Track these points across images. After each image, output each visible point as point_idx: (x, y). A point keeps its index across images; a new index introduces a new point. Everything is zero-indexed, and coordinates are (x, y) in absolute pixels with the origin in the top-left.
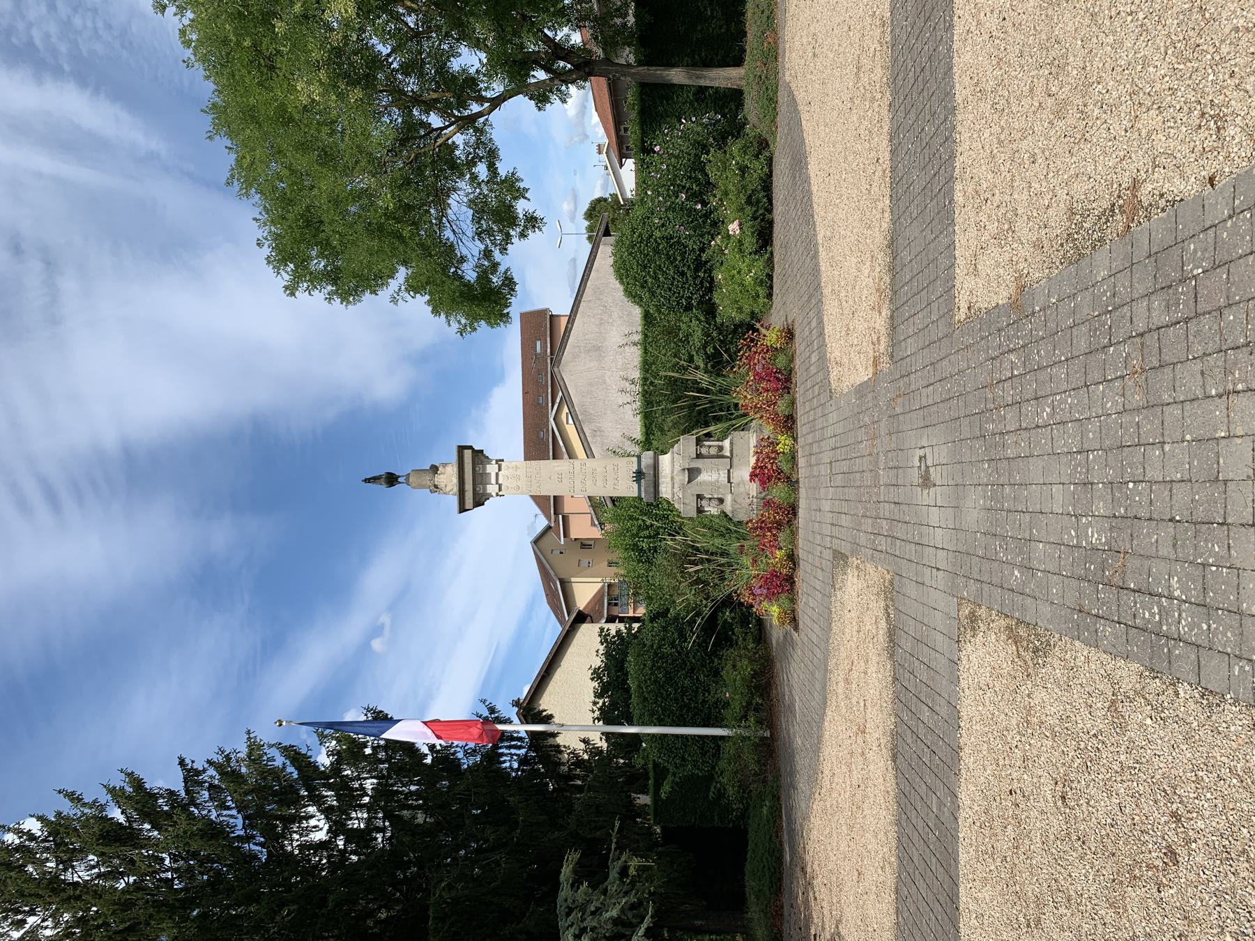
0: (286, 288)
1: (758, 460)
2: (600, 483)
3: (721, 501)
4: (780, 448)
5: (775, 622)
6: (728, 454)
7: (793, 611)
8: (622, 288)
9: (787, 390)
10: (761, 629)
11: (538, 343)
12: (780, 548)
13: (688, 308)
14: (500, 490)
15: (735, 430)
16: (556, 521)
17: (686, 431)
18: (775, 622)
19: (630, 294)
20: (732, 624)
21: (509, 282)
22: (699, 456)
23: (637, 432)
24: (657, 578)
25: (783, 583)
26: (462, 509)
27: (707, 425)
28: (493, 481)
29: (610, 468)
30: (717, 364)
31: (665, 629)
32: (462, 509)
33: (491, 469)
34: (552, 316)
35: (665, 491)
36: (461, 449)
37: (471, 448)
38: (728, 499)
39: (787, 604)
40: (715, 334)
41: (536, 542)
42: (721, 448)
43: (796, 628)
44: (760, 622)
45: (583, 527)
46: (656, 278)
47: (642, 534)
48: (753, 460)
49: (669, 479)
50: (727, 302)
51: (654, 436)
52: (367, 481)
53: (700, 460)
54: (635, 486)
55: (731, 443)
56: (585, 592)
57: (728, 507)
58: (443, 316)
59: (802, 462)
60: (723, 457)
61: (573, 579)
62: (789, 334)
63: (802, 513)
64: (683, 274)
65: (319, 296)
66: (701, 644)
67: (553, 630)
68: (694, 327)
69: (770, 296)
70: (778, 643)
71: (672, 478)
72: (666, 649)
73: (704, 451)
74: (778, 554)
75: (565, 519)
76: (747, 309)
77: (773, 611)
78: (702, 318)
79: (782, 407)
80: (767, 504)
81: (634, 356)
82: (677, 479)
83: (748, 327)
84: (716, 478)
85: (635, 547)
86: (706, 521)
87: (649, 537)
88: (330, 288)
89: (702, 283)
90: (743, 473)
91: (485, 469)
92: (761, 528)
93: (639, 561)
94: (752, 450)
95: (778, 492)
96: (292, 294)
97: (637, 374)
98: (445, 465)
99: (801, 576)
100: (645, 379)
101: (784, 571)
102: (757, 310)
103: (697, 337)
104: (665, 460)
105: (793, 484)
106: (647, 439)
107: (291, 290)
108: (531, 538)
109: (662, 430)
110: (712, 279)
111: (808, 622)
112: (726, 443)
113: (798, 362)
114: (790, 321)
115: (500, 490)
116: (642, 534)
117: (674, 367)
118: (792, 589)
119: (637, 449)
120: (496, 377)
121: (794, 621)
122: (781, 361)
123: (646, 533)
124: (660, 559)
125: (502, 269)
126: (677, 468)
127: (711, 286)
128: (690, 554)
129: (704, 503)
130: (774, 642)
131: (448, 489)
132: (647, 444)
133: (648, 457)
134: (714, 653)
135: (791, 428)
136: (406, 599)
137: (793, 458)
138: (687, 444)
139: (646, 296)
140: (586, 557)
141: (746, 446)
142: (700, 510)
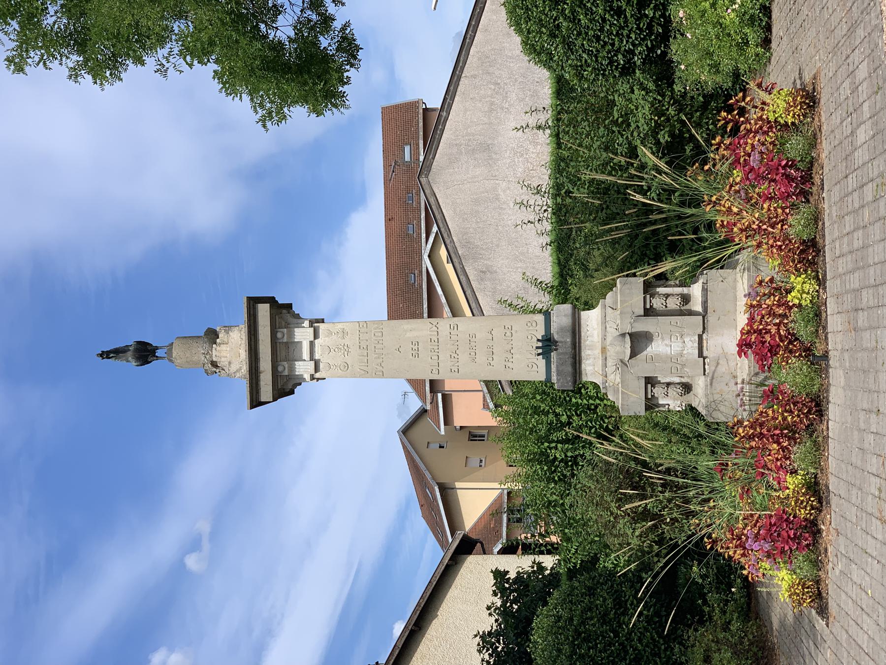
0: (10, 60)
1: (751, 319)
2: (481, 358)
3: (687, 388)
4: (793, 298)
5: (783, 595)
6: (698, 308)
7: (818, 582)
8: (518, 39)
9: (805, 195)
10: (751, 602)
11: (407, 149)
12: (794, 472)
13: (627, 70)
14: (317, 369)
15: (711, 267)
16: (434, 401)
17: (627, 267)
18: (783, 595)
19: (533, 49)
20: (702, 586)
21: (349, 47)
22: (649, 312)
23: (547, 272)
24: (581, 508)
25: (800, 534)
26: (256, 402)
27: (658, 259)
28: (306, 355)
29: (498, 333)
30: (680, 151)
31: (591, 591)
32: (256, 402)
33: (303, 335)
34: (426, 110)
35: (591, 371)
36: (253, 302)
37: (271, 301)
38: (700, 385)
39: (806, 570)
40: (672, 111)
41: (405, 431)
42: (686, 299)
43: (823, 611)
44: (749, 586)
45: (471, 411)
46: (574, 20)
47: (554, 437)
48: (742, 320)
49: (598, 351)
50: (693, 57)
51: (573, 280)
52: (105, 355)
53: (651, 320)
54: (541, 362)
55: (705, 291)
56: (476, 501)
57: (699, 398)
58: (246, 98)
59: (834, 322)
60: (691, 313)
61: (458, 485)
62: (808, 99)
63: (834, 412)
64: (619, 12)
65: (60, 69)
66: (654, 620)
67: (431, 555)
68: (638, 102)
69: (766, 42)
70: (782, 623)
71: (604, 350)
72: (593, 626)
73: (657, 303)
74: (792, 482)
75: (446, 399)
76: (727, 65)
77: (780, 582)
78: (651, 86)
79: (797, 225)
80: (771, 395)
81: (539, 151)
82: (612, 352)
83: (723, 103)
84: (686, 349)
85: (542, 458)
86: (658, 418)
87: (566, 441)
88: (75, 57)
89: (650, 27)
90: (725, 340)
91: (291, 335)
92: (761, 436)
93: (550, 480)
94: (742, 302)
95: (791, 374)
96: (20, 69)
97: (543, 177)
98: (228, 328)
99: (832, 525)
100: (558, 188)
101: (802, 514)
102: (742, 67)
103: (643, 115)
104: (591, 319)
105: (818, 362)
106: (561, 284)
107: (17, 64)
108: (400, 424)
109: (585, 269)
110: (668, 21)
111: (850, 607)
112: (696, 290)
113: (825, 148)
114: (807, 78)
115: (317, 369)
116: (554, 437)
117: (603, 167)
118: (815, 543)
119: (543, 300)
120: (358, 200)
121: (819, 600)
122: (795, 146)
123: (561, 435)
124: (584, 476)
125: (337, 24)
126: (612, 333)
127: (666, 31)
128: (633, 477)
129: (658, 391)
130: (776, 624)
131: (234, 368)
132: (562, 290)
133: (562, 314)
134: (674, 636)
135: (813, 263)
136: (239, 501)
137: (817, 315)
138: (628, 293)
139: (558, 51)
140: (476, 451)
141: (730, 295)
142: (651, 404)
